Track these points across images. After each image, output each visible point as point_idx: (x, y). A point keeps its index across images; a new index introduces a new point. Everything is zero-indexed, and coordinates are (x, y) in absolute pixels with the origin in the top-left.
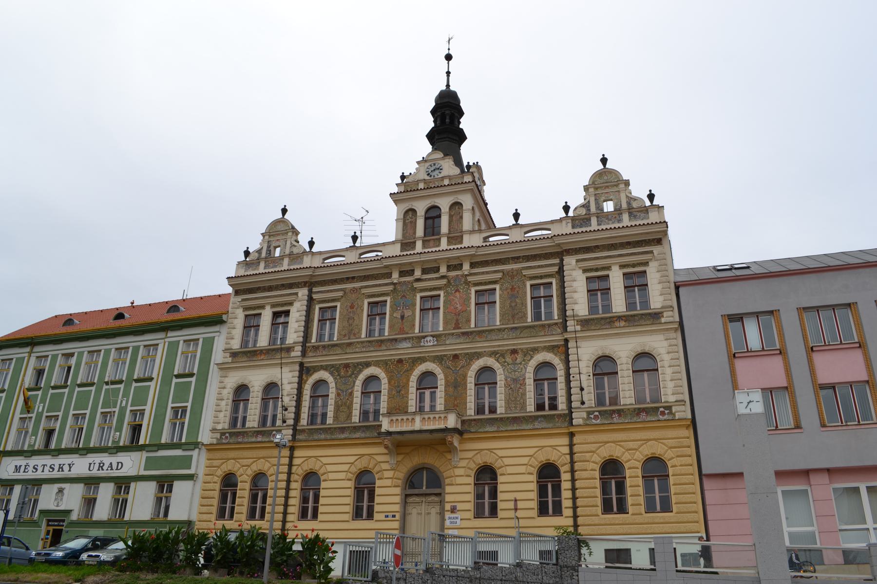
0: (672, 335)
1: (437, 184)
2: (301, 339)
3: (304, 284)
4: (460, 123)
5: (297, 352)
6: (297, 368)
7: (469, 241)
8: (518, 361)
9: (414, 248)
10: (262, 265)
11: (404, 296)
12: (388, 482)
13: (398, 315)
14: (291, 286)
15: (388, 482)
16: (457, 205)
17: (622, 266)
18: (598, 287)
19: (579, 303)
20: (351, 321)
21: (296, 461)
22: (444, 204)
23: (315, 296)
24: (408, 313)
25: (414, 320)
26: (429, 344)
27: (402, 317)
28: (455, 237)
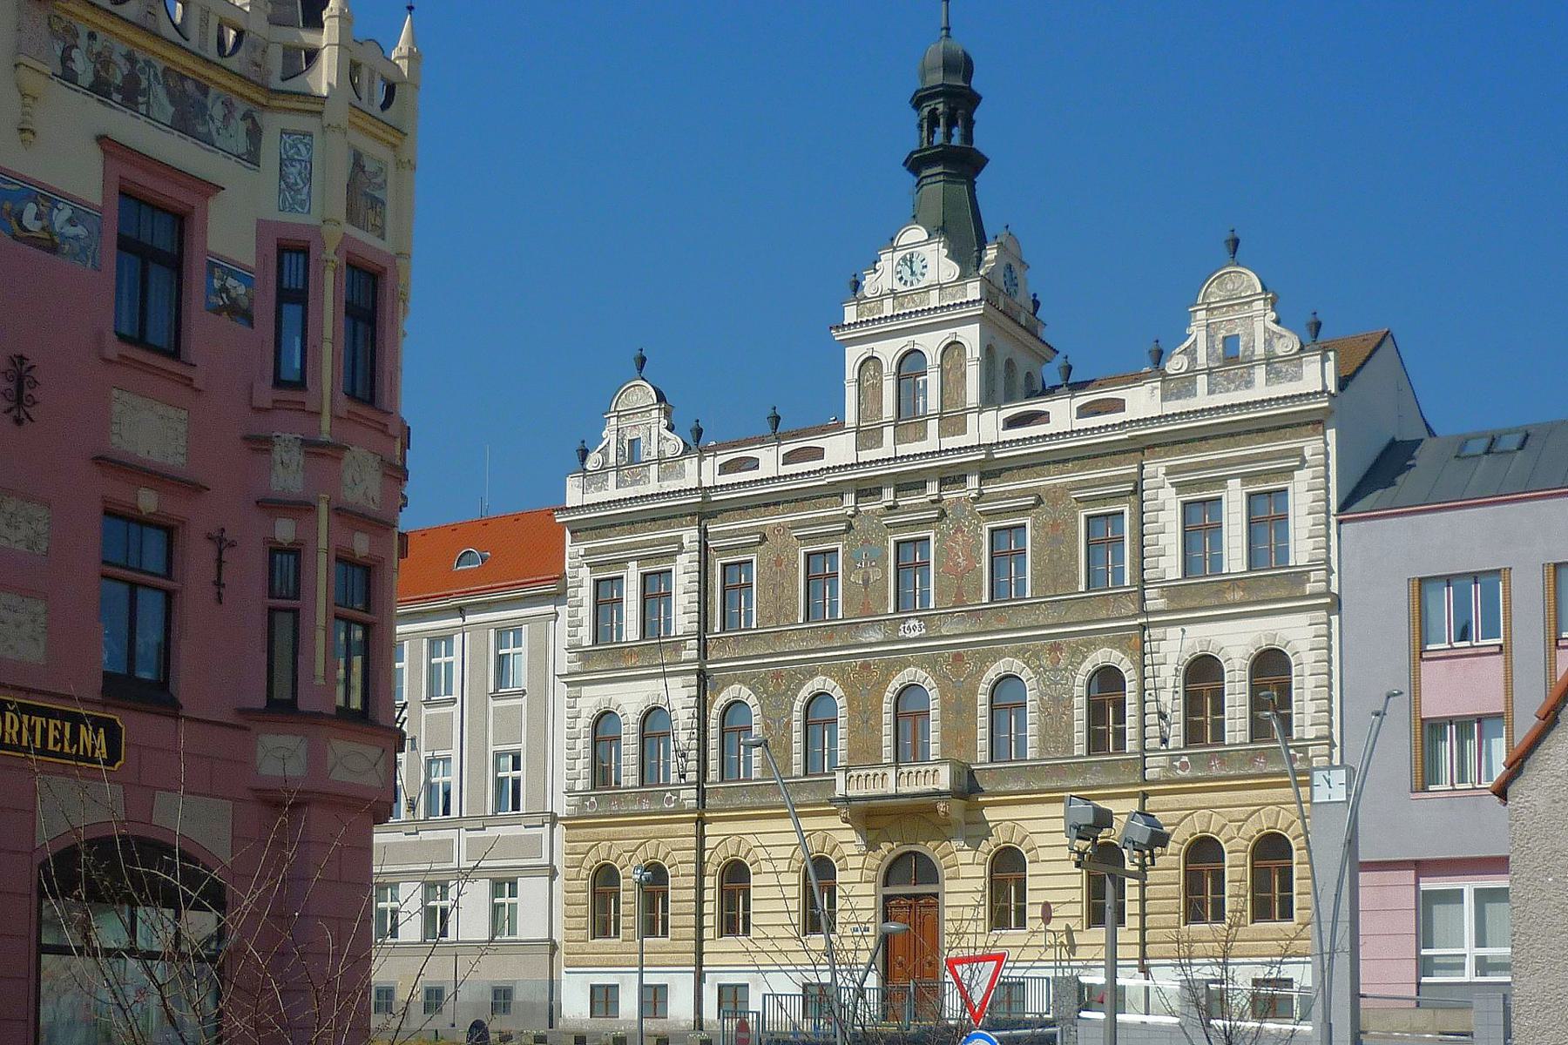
8: (1062, 664)
11: (866, 541)
12: (856, 876)
15: (856, 876)
18: (1200, 525)
21: (709, 843)
22: (931, 344)
24: (875, 575)
27: (866, 582)
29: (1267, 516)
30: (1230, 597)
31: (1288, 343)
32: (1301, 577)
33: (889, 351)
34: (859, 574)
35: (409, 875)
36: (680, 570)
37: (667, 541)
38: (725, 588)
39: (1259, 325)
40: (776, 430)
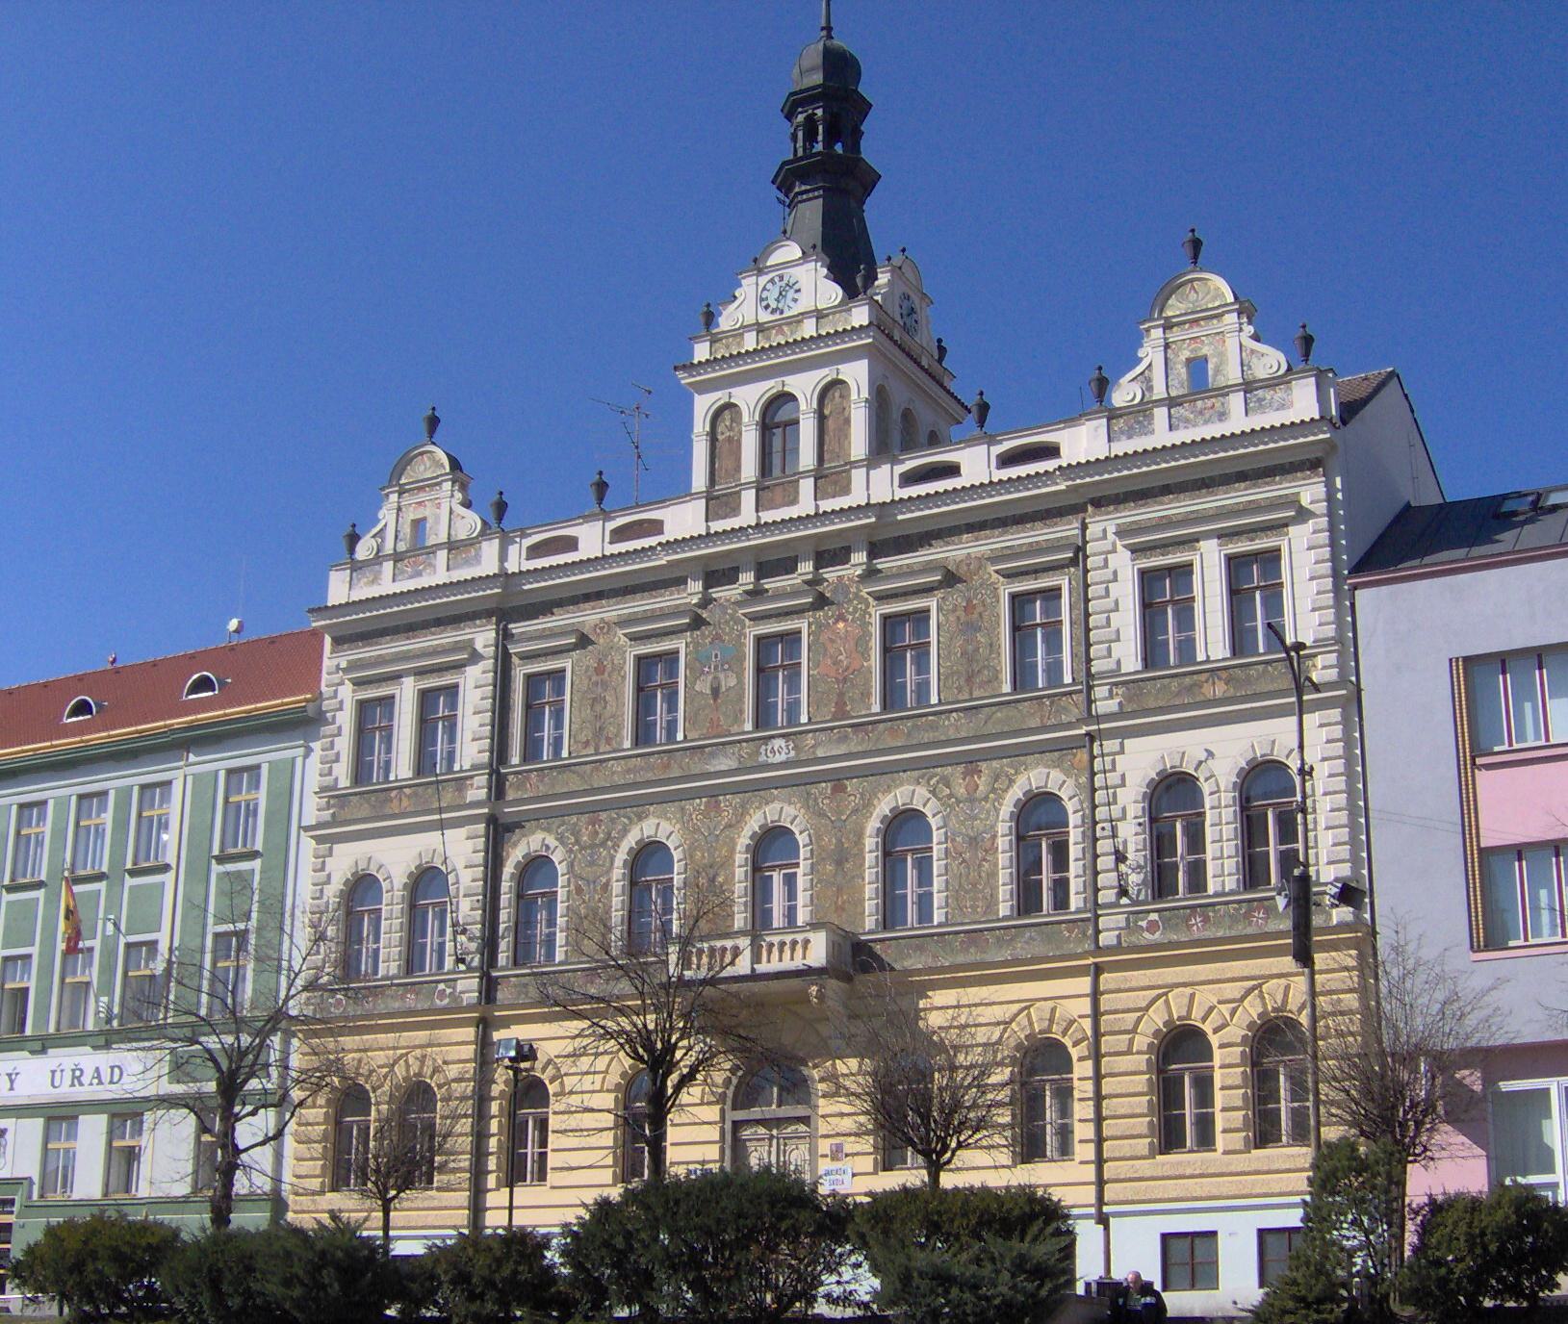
3: (487, 614)
13: (703, 686)
18: (1163, 593)
20: (598, 708)
22: (804, 386)
24: (728, 681)
27: (716, 692)
29: (1253, 578)
30: (1208, 691)
33: (749, 398)
34: (713, 680)
38: (525, 705)
39: (1235, 348)
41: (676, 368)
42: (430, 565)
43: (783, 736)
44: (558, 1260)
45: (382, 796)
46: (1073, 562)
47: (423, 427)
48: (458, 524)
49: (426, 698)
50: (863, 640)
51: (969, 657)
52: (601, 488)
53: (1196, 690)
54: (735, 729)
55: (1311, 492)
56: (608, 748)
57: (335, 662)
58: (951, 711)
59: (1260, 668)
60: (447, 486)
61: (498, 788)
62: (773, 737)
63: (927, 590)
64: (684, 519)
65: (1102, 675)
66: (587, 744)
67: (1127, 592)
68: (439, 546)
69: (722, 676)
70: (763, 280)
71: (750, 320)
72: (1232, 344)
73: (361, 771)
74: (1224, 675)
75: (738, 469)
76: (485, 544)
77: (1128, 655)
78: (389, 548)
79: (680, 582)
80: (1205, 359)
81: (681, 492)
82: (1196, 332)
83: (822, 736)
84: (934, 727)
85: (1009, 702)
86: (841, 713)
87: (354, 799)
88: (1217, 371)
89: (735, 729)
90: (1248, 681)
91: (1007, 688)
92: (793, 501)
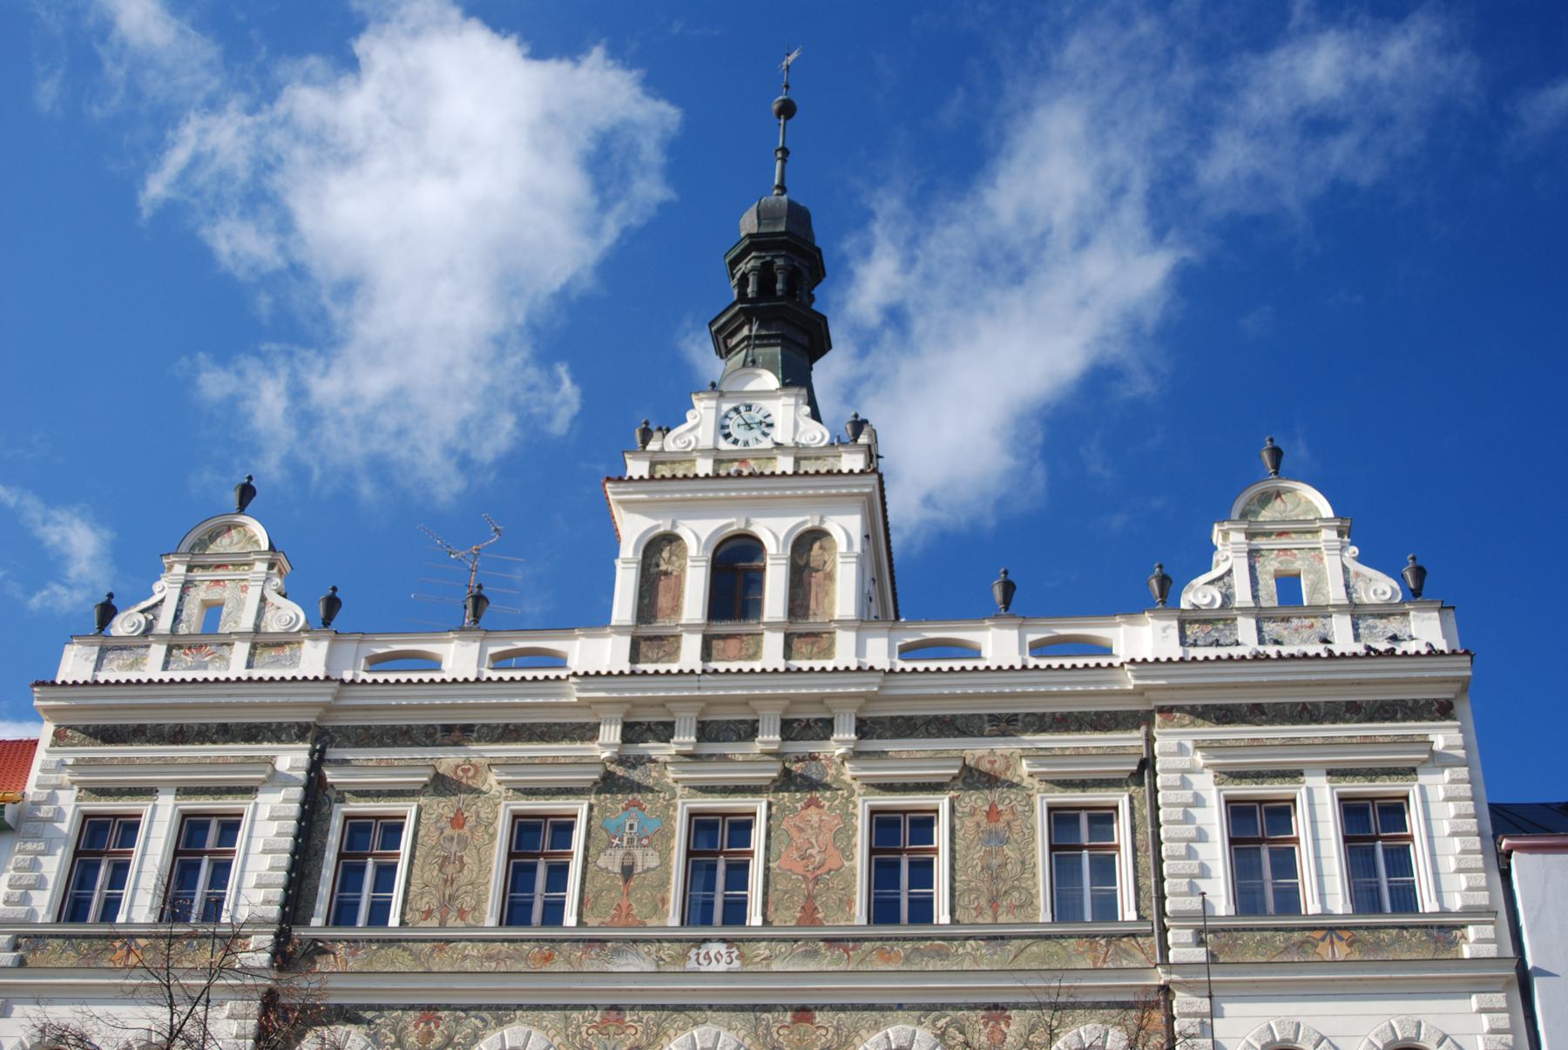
0: (1499, 1000)
1: (754, 466)
2: (274, 912)
3: (300, 732)
4: (812, 299)
5: (257, 953)
6: (255, 1007)
7: (844, 652)
9: (673, 655)
10: (157, 652)
13: (610, 861)
14: (252, 733)
16: (807, 543)
17: (1334, 773)
18: (1258, 830)
19: (1206, 873)
20: (450, 870)
22: (774, 533)
23: (331, 775)
24: (647, 860)
25: (664, 884)
26: (714, 967)
27: (628, 871)
28: (804, 631)
29: (1374, 829)
30: (1325, 952)
31: (287, 614)
32: (1445, 930)
33: (698, 534)
34: (628, 860)
35: (781, 298)
36: (264, 812)
37: (248, 762)
38: (342, 858)
39: (1331, 566)
40: (477, 612)
41: (609, 479)
42: (221, 657)
43: (723, 940)
44: (879, 652)
45: (99, 944)
46: (1137, 777)
47: (233, 497)
48: (269, 614)
49: (191, 829)
50: (847, 831)
51: (994, 873)
52: (479, 601)
53: (1308, 947)
54: (653, 922)
55: (1444, 736)
56: (460, 923)
57: (57, 758)
58: (968, 938)
59: (1394, 932)
60: (261, 567)
61: (286, 955)
62: (706, 940)
63: (936, 787)
64: (599, 652)
65: (1181, 916)
66: (428, 914)
67: (1213, 819)
68: (242, 635)
69: (638, 853)
70: (726, 407)
71: (707, 442)
72: (1331, 565)
73: (73, 907)
74: (1346, 935)
75: (676, 608)
76: (307, 645)
77: (1220, 897)
78: (164, 624)
79: (588, 732)
80: (1296, 578)
81: (595, 619)
82: (1283, 543)
83: (783, 947)
84: (942, 954)
85: (1048, 937)
86: (809, 916)
87: (56, 942)
88: (1315, 589)
89: (653, 922)
90: (1378, 946)
91: (1044, 916)
92: (755, 656)
